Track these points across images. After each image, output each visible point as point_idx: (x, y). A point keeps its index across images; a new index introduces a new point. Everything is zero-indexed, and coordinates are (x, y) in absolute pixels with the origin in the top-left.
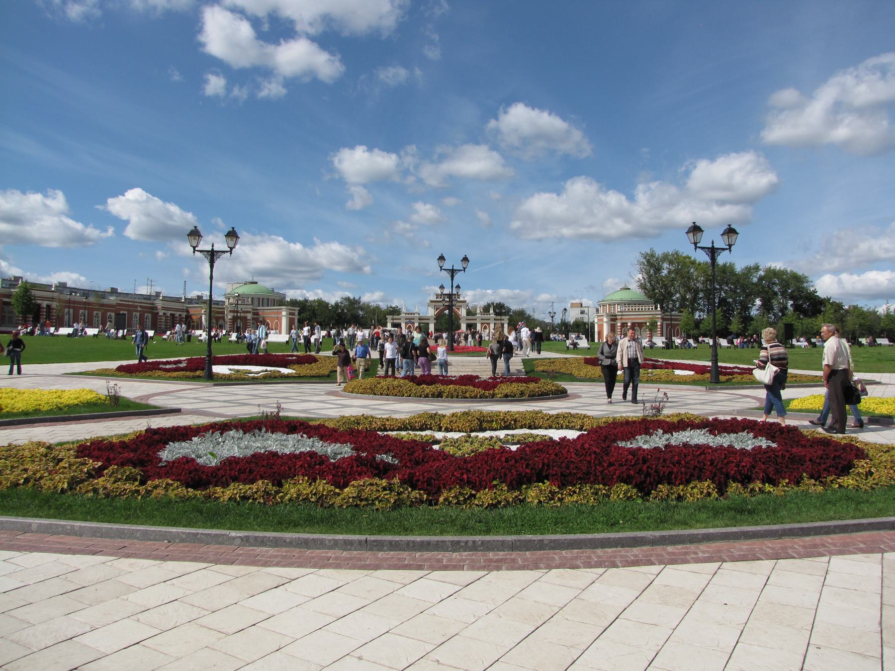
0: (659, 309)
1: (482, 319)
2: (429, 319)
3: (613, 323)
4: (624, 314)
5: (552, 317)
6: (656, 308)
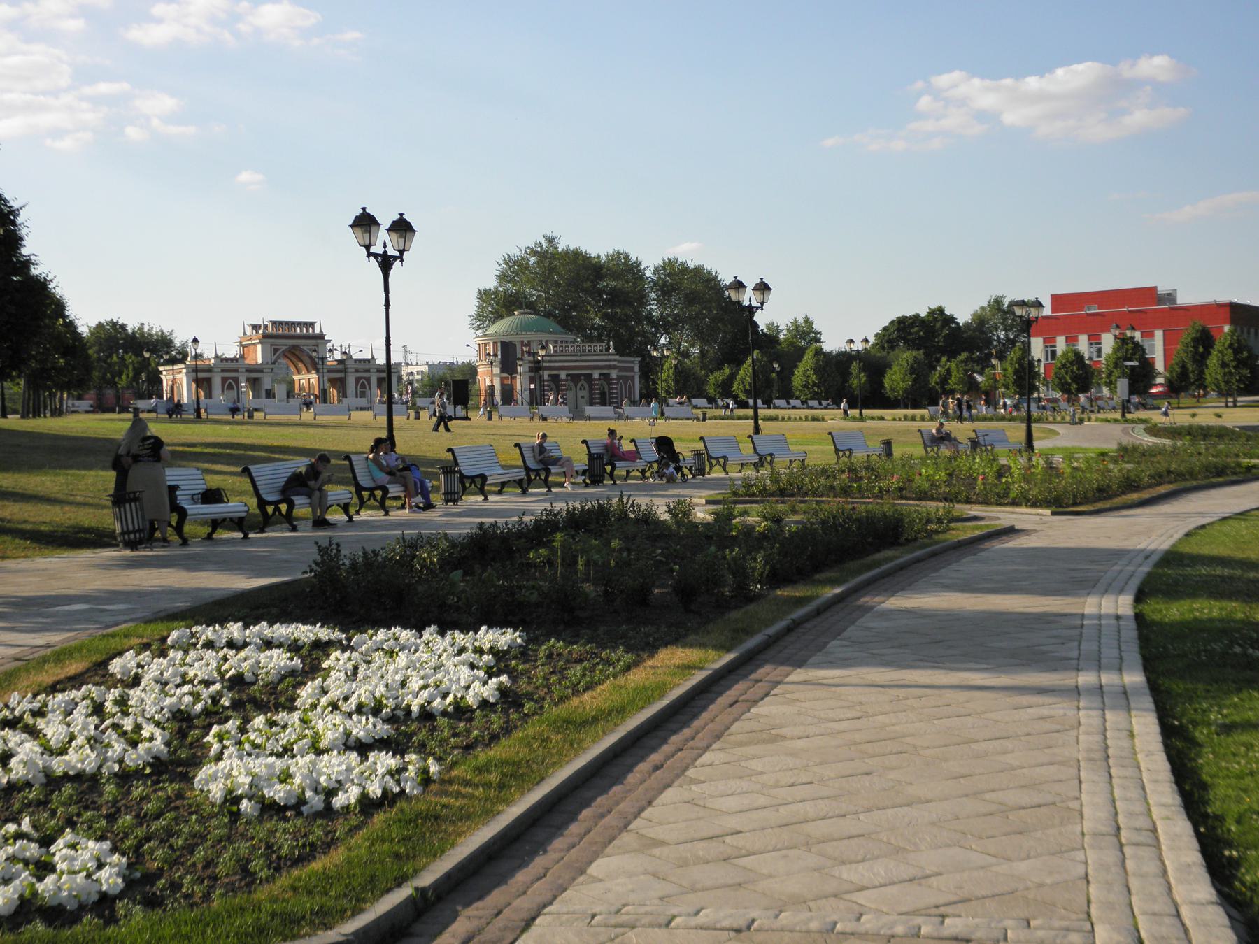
0: (611, 349)
1: (223, 371)
2: (261, 371)
3: (532, 374)
4: (553, 358)
5: (386, 263)
6: (608, 349)
